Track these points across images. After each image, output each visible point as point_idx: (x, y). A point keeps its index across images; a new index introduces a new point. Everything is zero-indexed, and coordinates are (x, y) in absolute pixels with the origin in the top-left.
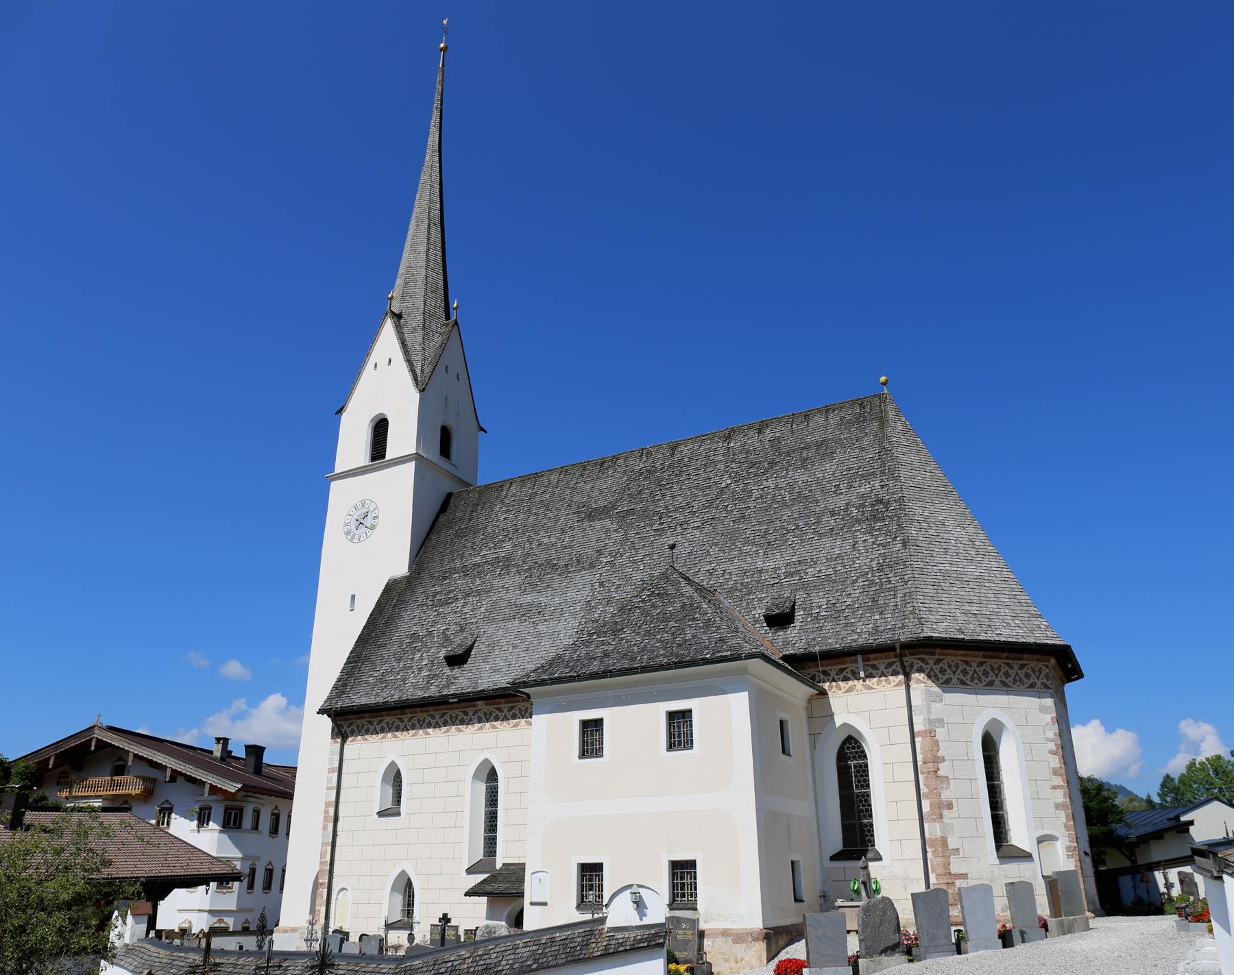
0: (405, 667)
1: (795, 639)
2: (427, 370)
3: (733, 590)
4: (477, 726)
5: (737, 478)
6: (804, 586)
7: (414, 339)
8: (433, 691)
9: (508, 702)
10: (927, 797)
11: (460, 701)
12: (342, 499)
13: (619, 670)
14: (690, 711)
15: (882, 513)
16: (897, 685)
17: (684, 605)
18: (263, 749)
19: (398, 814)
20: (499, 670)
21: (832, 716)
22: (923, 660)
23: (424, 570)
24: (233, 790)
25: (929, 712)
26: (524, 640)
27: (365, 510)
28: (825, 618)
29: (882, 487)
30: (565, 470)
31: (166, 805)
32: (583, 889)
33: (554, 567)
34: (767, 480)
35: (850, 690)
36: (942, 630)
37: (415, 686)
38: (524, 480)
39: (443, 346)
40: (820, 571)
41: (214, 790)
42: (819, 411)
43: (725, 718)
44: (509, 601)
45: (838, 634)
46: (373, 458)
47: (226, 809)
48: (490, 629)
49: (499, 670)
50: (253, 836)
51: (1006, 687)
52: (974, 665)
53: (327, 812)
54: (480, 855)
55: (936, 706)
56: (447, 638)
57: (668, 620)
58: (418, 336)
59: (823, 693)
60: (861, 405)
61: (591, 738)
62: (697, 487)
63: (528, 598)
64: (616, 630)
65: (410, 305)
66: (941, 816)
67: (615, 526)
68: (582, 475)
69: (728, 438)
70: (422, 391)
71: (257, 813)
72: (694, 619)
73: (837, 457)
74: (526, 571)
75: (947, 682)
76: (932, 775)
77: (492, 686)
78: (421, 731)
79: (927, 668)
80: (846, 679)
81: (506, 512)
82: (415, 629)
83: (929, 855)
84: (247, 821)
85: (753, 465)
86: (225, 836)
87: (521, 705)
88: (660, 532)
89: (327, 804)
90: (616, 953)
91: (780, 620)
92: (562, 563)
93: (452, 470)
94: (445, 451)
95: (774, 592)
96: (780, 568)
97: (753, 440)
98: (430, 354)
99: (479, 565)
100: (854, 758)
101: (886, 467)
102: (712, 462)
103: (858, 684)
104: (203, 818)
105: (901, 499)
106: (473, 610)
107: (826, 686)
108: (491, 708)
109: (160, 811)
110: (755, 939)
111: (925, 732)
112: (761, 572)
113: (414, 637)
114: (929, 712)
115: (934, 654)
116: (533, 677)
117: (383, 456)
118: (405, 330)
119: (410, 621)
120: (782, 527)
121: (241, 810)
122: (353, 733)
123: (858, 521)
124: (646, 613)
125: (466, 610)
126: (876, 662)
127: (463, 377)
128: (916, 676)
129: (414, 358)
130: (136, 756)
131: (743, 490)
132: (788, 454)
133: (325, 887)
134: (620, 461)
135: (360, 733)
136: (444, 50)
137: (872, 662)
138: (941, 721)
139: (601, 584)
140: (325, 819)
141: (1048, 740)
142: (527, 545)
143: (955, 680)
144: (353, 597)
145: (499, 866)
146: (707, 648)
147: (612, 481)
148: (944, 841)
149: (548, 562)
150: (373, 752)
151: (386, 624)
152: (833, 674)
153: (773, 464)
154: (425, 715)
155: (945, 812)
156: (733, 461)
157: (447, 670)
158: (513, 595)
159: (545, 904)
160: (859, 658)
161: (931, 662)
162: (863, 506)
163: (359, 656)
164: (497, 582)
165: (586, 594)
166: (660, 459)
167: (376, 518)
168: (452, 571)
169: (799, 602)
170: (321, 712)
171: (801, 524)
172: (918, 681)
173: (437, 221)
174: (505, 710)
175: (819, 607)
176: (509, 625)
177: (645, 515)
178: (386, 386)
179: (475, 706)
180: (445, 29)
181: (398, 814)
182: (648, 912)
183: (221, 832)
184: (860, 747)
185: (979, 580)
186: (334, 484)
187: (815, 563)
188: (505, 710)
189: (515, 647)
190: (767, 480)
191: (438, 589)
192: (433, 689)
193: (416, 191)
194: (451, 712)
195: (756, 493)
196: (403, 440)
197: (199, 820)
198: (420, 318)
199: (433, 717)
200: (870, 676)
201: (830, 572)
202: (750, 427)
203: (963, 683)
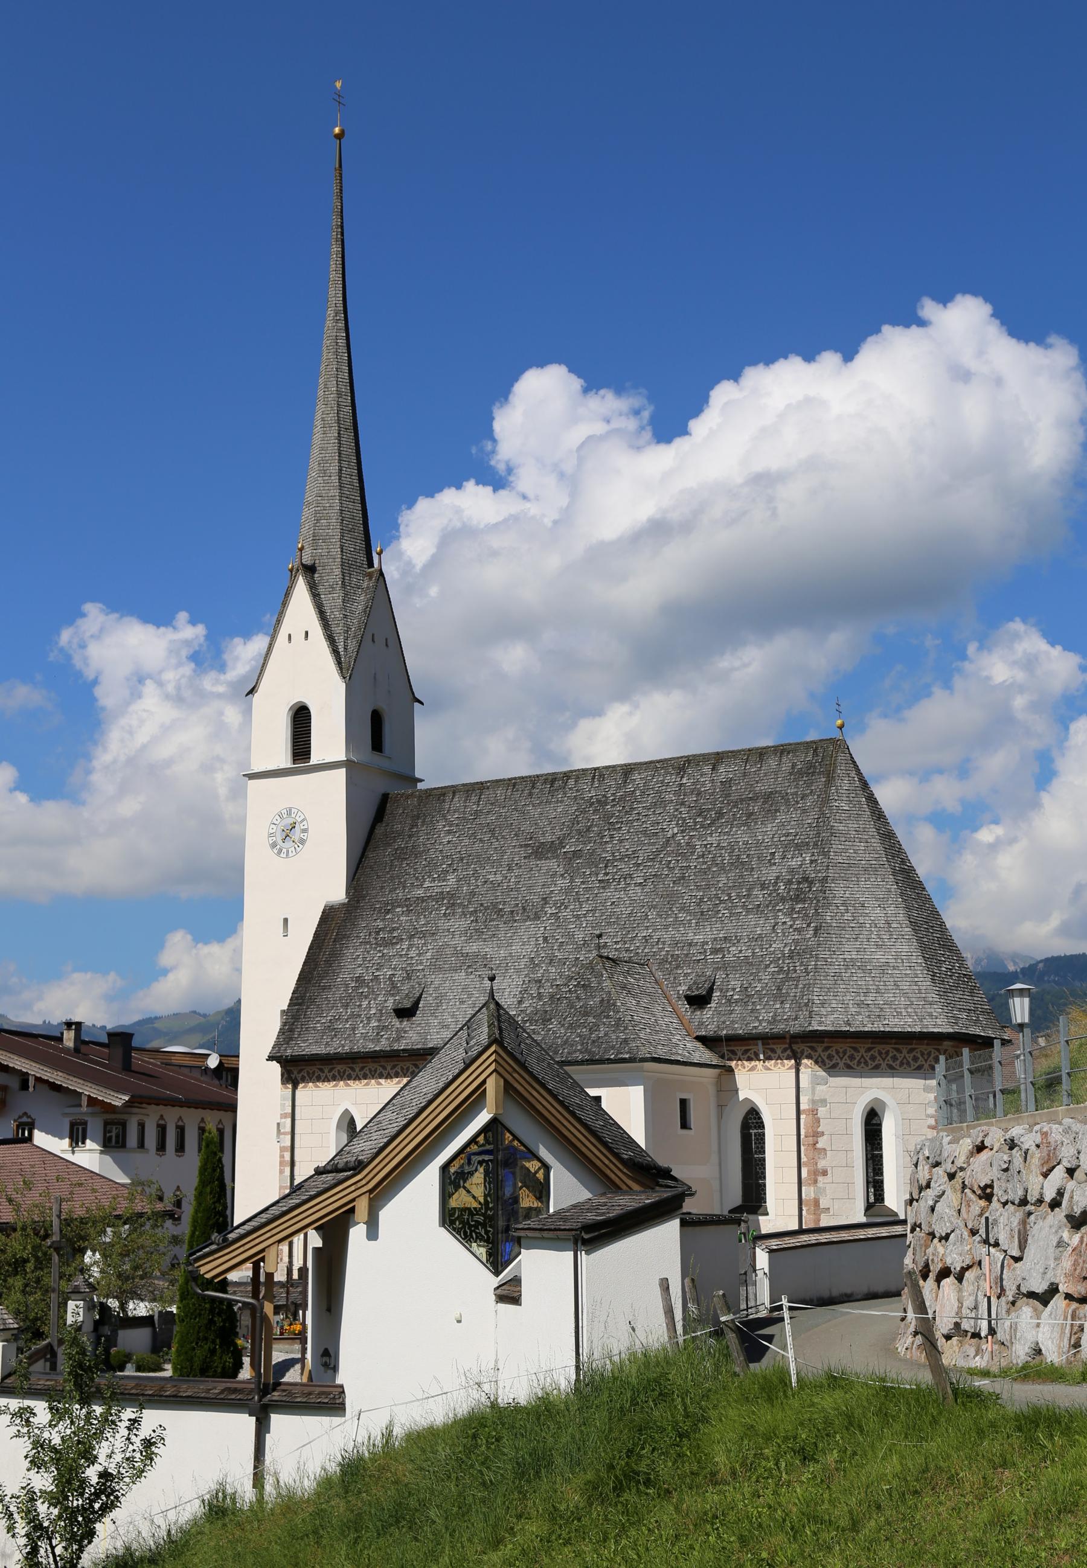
0: (352, 1016)
1: (709, 1020)
2: (352, 645)
3: (664, 961)
6: (724, 966)
7: (333, 600)
8: (383, 1045)
10: (806, 1165)
14: (600, 1097)
15: (805, 894)
16: (789, 1068)
17: (602, 1001)
18: (132, 1035)
21: (737, 1090)
22: (812, 1048)
24: (118, 1103)
25: (813, 1093)
26: (470, 996)
27: (291, 821)
29: (812, 862)
31: (25, 1119)
35: (752, 1069)
36: (827, 1021)
37: (365, 1036)
40: (741, 951)
41: (92, 1101)
47: (106, 1124)
48: (436, 979)
50: (138, 1157)
51: (892, 1070)
52: (862, 1051)
53: (282, 1156)
55: (819, 1088)
56: (394, 986)
57: (586, 1014)
59: (731, 1070)
60: (815, 750)
62: (644, 832)
66: (816, 1181)
68: (531, 794)
71: (142, 1126)
72: (608, 1017)
73: (781, 817)
74: (471, 913)
75: (834, 1066)
76: (811, 1147)
79: (815, 1055)
80: (749, 1059)
81: (449, 832)
82: (359, 971)
83: (804, 1213)
84: (132, 1140)
86: (108, 1159)
88: (604, 884)
89: (282, 1149)
91: (698, 1001)
94: (377, 744)
100: (755, 1127)
101: (820, 841)
103: (759, 1064)
104: (77, 1137)
105: (825, 880)
106: (419, 955)
107: (733, 1064)
109: (18, 1127)
111: (808, 1110)
112: (690, 945)
113: (359, 980)
114: (813, 1093)
115: (823, 1042)
118: (321, 589)
119: (354, 960)
121: (123, 1125)
122: (303, 1080)
123: (783, 900)
124: (571, 1006)
126: (774, 1047)
128: (805, 1061)
130: (38, 1080)
134: (571, 782)
135: (311, 1080)
137: (771, 1046)
138: (824, 1102)
139: (545, 939)
140: (282, 1163)
141: (928, 1116)
143: (841, 1065)
144: (286, 920)
146: (613, 1047)
148: (816, 1202)
149: (495, 905)
151: (329, 963)
152: (739, 1053)
153: (720, 814)
154: (376, 1065)
155: (820, 1178)
156: (683, 804)
157: (396, 1022)
158: (458, 941)
160: (760, 1042)
161: (820, 1050)
162: (790, 882)
163: (303, 997)
164: (443, 924)
167: (305, 831)
168: (395, 904)
170: (271, 1058)
172: (807, 1066)
173: (349, 422)
175: (734, 989)
177: (593, 860)
180: (339, 98)
183: (102, 1152)
184: (760, 1118)
185: (883, 968)
189: (462, 1003)
191: (381, 924)
192: (383, 1042)
194: (401, 1064)
196: (330, 739)
197: (71, 1138)
198: (338, 572)
199: (384, 1068)
200: (769, 1058)
201: (749, 953)
203: (849, 1067)
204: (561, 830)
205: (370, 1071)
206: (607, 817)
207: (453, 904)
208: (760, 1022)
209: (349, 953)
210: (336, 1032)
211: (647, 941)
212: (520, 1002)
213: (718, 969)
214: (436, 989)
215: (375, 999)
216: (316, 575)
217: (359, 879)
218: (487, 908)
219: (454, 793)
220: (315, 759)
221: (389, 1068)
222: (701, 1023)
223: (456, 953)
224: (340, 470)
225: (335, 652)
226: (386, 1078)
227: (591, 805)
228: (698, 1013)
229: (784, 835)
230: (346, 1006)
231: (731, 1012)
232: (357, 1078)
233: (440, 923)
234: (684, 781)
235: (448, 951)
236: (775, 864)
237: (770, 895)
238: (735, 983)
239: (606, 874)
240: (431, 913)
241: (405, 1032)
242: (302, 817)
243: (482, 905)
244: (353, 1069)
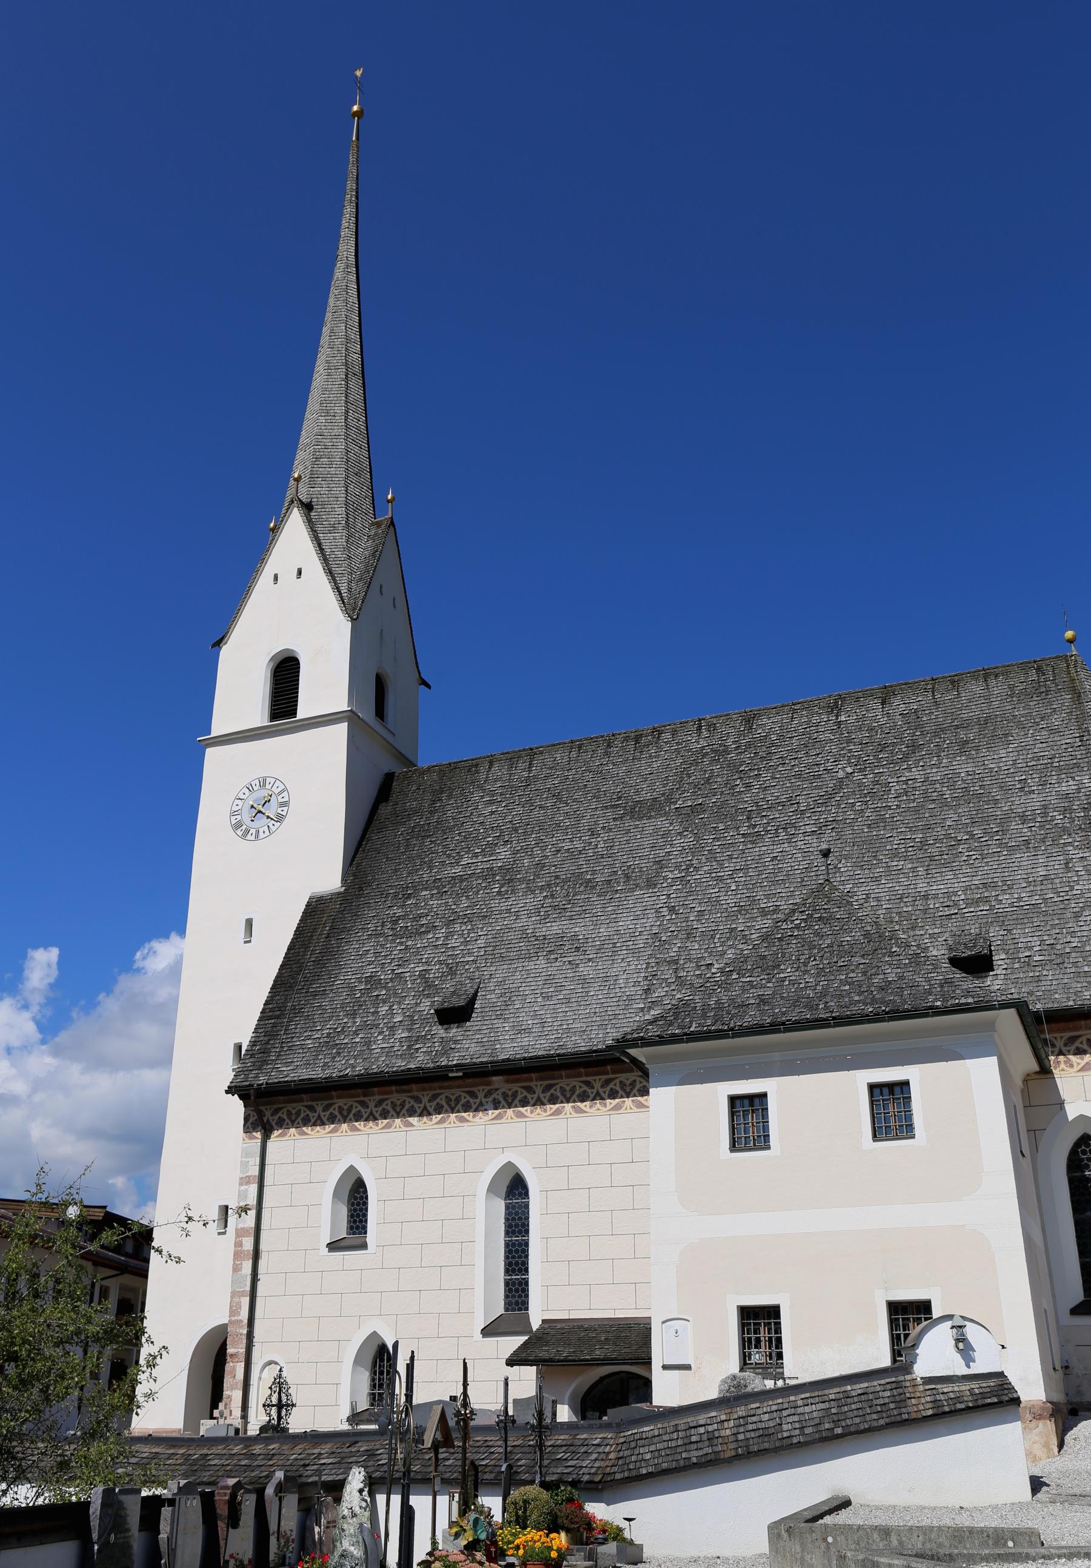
4: (492, 1113)
6: (999, 919)
7: (335, 541)
8: (421, 1060)
9: (607, 1071)
11: (466, 1076)
12: (225, 776)
13: (797, 1022)
14: (906, 1083)
19: (364, 1246)
20: (528, 1031)
21: (1061, 1104)
23: (369, 884)
28: (1042, 964)
32: (747, 1344)
33: (590, 885)
34: (909, 769)
37: (389, 1052)
38: (512, 758)
39: (377, 554)
40: (1020, 899)
42: (974, 675)
43: (965, 1095)
44: (524, 932)
45: (1066, 987)
46: (274, 715)
48: (500, 971)
49: (528, 1031)
54: (499, 1309)
56: (428, 984)
59: (1045, 1071)
60: (1039, 669)
61: (748, 1122)
62: (799, 776)
63: (555, 928)
64: (769, 966)
65: (324, 491)
69: (835, 708)
70: (352, 620)
74: (542, 888)
77: (521, 1054)
81: (491, 802)
82: (370, 970)
85: (883, 747)
87: (627, 1077)
88: (754, 838)
90: (749, 1455)
92: (599, 878)
93: (390, 739)
94: (380, 712)
95: (952, 925)
96: (955, 893)
97: (875, 711)
98: (358, 564)
102: (816, 741)
108: (515, 1087)
110: (1038, 1417)
113: (372, 981)
116: (653, 1031)
117: (294, 713)
118: (319, 528)
119: (359, 958)
120: (948, 836)
122: (281, 1124)
127: (401, 602)
129: (336, 570)
132: (936, 734)
133: (214, 1363)
135: (293, 1123)
136: (359, 114)
139: (672, 910)
140: (238, 1255)
142: (537, 851)
144: (249, 923)
145: (535, 1324)
150: (314, 1157)
151: (320, 963)
153: (914, 747)
154: (403, 1097)
157: (440, 1031)
159: (687, 1367)
163: (281, 1009)
165: (650, 921)
166: (730, 734)
168: (416, 888)
170: (230, 1091)
171: (977, 832)
173: (357, 369)
174: (539, 1090)
176: (531, 965)
177: (721, 812)
178: (295, 605)
179: (488, 1084)
181: (364, 1246)
182: (976, 1355)
186: (209, 751)
187: (1010, 887)
188: (539, 1090)
191: (399, 912)
193: (321, 324)
194: (447, 1093)
195: (895, 788)
196: (326, 687)
199: (418, 1100)
202: (869, 694)
204: (665, 786)
205: (394, 1105)
206: (734, 768)
207: (511, 880)
209: (352, 949)
210: (340, 1049)
212: (647, 991)
214: (499, 984)
215: (399, 1003)
216: (313, 514)
217: (359, 864)
218: (565, 881)
219: (491, 763)
220: (303, 712)
221: (425, 1100)
223: (524, 936)
224: (347, 412)
225: (337, 589)
227: (704, 756)
229: (1032, 759)
230: (354, 1015)
232: (372, 1117)
233: (494, 904)
234: (843, 718)
235: (512, 935)
240: (477, 893)
241: (456, 1042)
242: (282, 787)
243: (557, 877)
244: (364, 1104)
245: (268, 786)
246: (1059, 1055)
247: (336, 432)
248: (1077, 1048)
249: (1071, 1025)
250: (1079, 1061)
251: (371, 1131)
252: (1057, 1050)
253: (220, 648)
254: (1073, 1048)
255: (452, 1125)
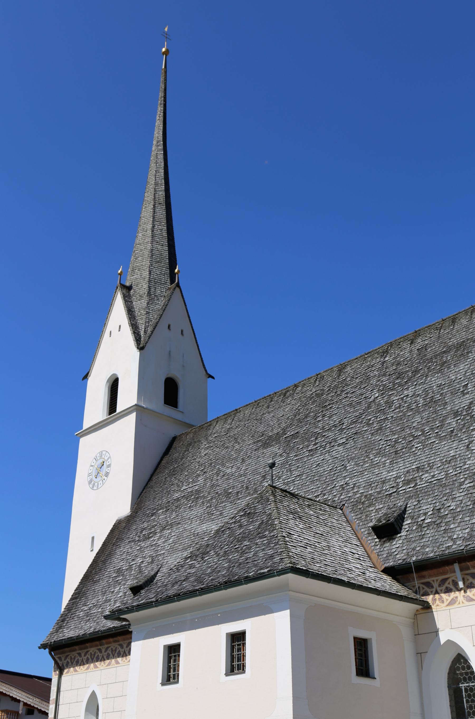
1: (399, 550)
3: (359, 501)
4: (107, 662)
5: (384, 390)
6: (416, 494)
7: (140, 305)
21: (436, 632)
27: (101, 461)
30: (257, 403)
35: (452, 603)
40: (433, 476)
56: (140, 571)
58: (144, 302)
59: (427, 607)
62: (350, 405)
67: (280, 451)
69: (385, 352)
70: (141, 348)
78: (113, 660)
80: (448, 591)
91: (387, 531)
96: (400, 477)
98: (154, 317)
99: (178, 500)
100: (465, 679)
103: (460, 595)
107: (429, 599)
112: (384, 482)
117: (115, 411)
125: (160, 542)
127: (188, 331)
131: (386, 402)
136: (166, 53)
144: (93, 538)
147: (287, 409)
152: (436, 585)
153: (416, 372)
156: (384, 375)
169: (409, 511)
180: (166, 36)
186: (83, 441)
190: (407, 389)
191: (145, 525)
196: (128, 397)
198: (146, 286)
208: (454, 541)
211: (343, 489)
213: (410, 498)
216: (132, 291)
222: (390, 554)
224: (153, 227)
226: (123, 657)
228: (387, 544)
231: (422, 537)
232: (82, 663)
236: (468, 393)
237: (463, 420)
238: (427, 508)
239: (316, 444)
242: (108, 456)
245: (103, 457)
246: (435, 594)
247: (147, 240)
248: (447, 588)
249: (441, 570)
250: (447, 597)
251: (102, 668)
252: (434, 590)
253: (88, 379)
254: (444, 588)
255: (461, 605)
